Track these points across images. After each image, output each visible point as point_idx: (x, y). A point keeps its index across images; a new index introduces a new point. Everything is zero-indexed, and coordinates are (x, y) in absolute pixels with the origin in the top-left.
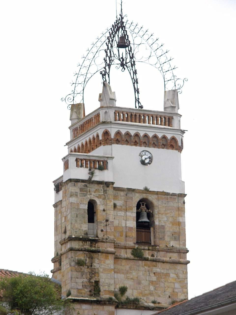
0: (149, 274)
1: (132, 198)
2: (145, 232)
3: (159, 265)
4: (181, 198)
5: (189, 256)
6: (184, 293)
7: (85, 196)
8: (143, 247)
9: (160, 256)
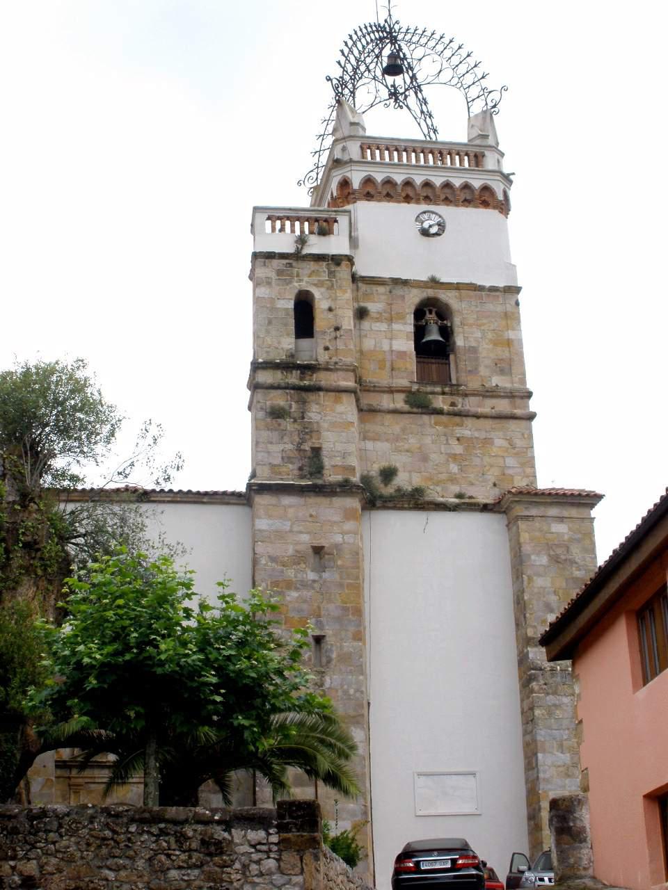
0: (447, 440)
1: (404, 298)
2: (438, 363)
3: (469, 422)
4: (510, 296)
5: (533, 405)
6: (528, 477)
7: (287, 284)
8: (429, 389)
9: (471, 404)
